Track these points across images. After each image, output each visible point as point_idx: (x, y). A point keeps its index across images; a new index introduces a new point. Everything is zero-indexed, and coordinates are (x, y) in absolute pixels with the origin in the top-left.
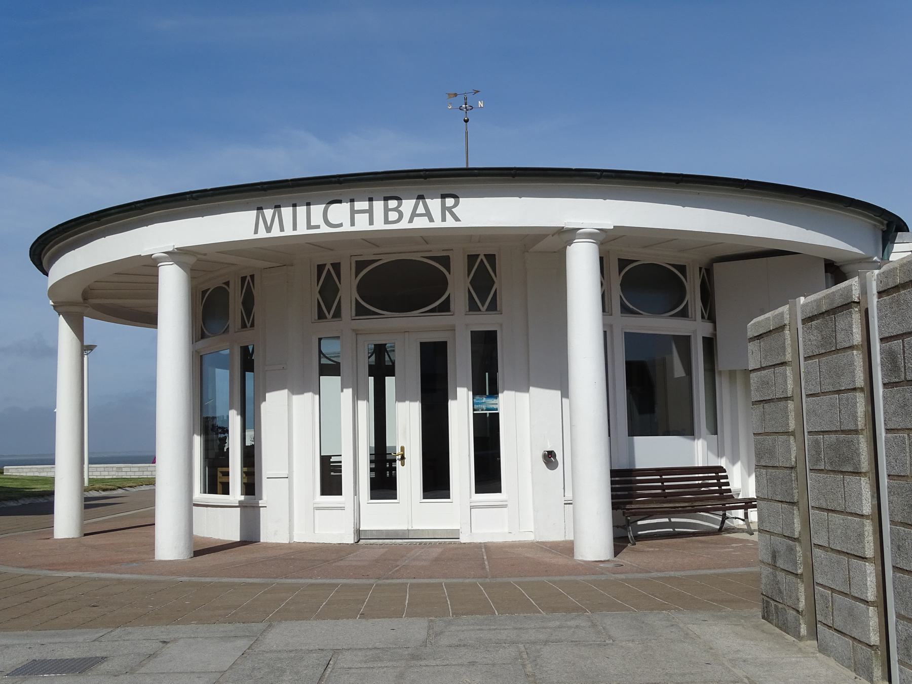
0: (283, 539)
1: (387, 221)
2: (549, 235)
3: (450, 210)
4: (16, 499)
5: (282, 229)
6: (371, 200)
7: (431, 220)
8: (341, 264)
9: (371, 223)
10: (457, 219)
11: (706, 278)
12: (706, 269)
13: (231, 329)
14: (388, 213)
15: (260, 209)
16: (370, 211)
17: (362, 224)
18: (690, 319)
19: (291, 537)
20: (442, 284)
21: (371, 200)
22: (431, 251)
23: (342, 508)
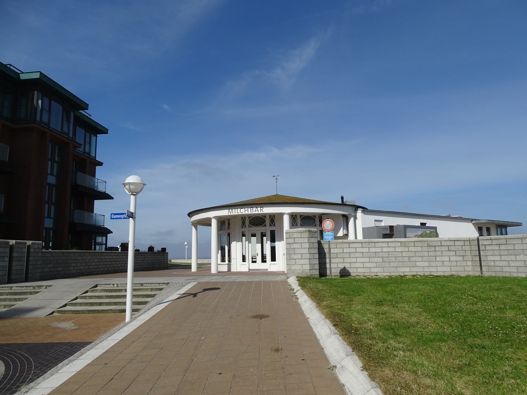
0: (235, 271)
1: (251, 212)
3: (262, 210)
4: (179, 267)
5: (233, 213)
6: (248, 208)
7: (258, 212)
9: (248, 212)
13: (226, 229)
15: (229, 209)
16: (248, 210)
17: (247, 213)
19: (237, 270)
20: (264, 221)
21: (248, 208)
23: (246, 265)
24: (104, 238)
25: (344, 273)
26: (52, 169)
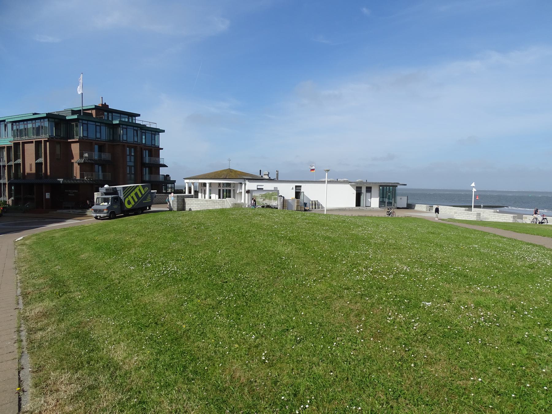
24: (173, 185)
25: (190, 210)
26: (130, 159)
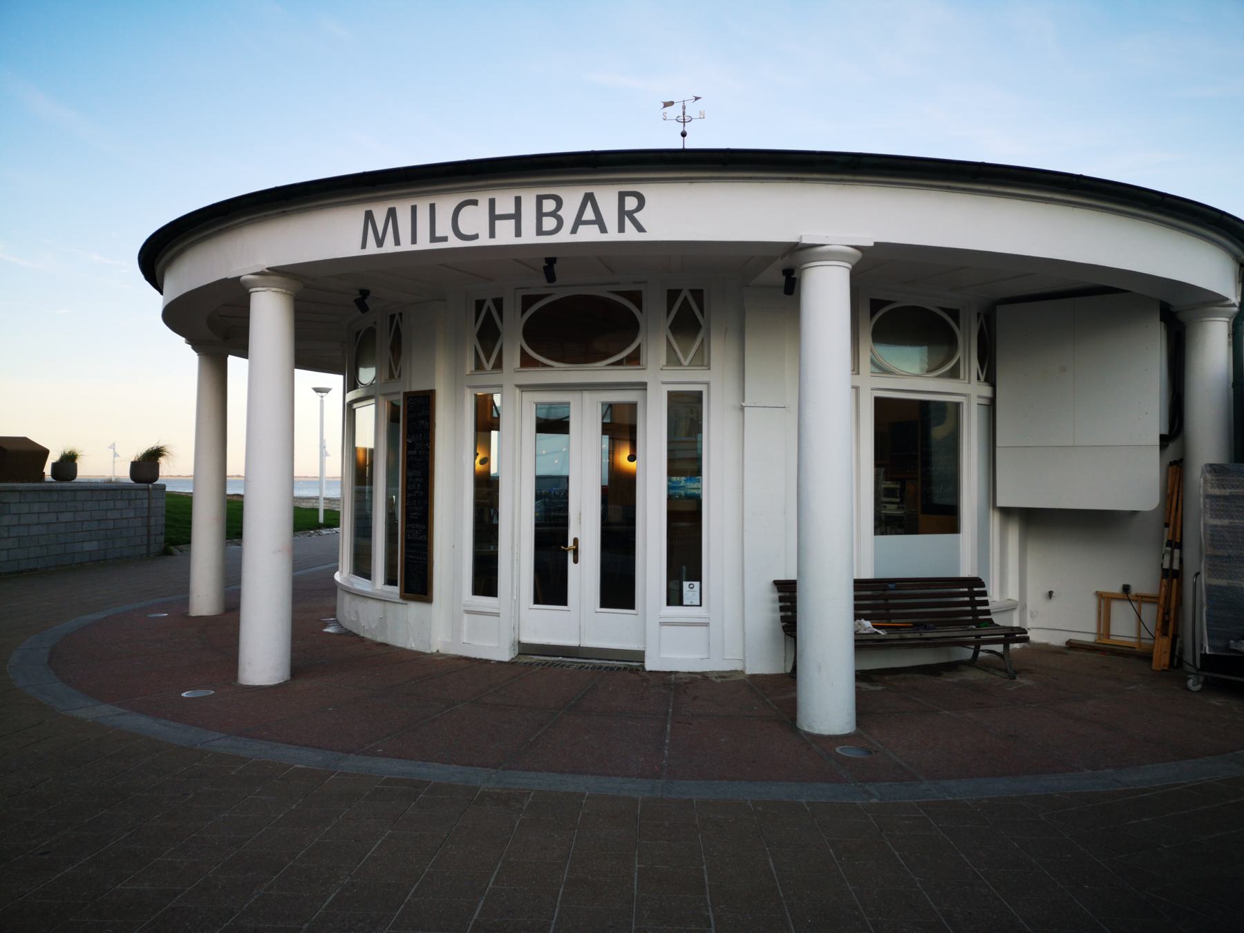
1: (540, 232)
2: (778, 257)
3: (630, 214)
5: (397, 242)
7: (603, 229)
8: (493, 297)
10: (640, 229)
11: (986, 331)
12: (985, 316)
14: (516, 211)
18: (961, 381)
22: (617, 284)
